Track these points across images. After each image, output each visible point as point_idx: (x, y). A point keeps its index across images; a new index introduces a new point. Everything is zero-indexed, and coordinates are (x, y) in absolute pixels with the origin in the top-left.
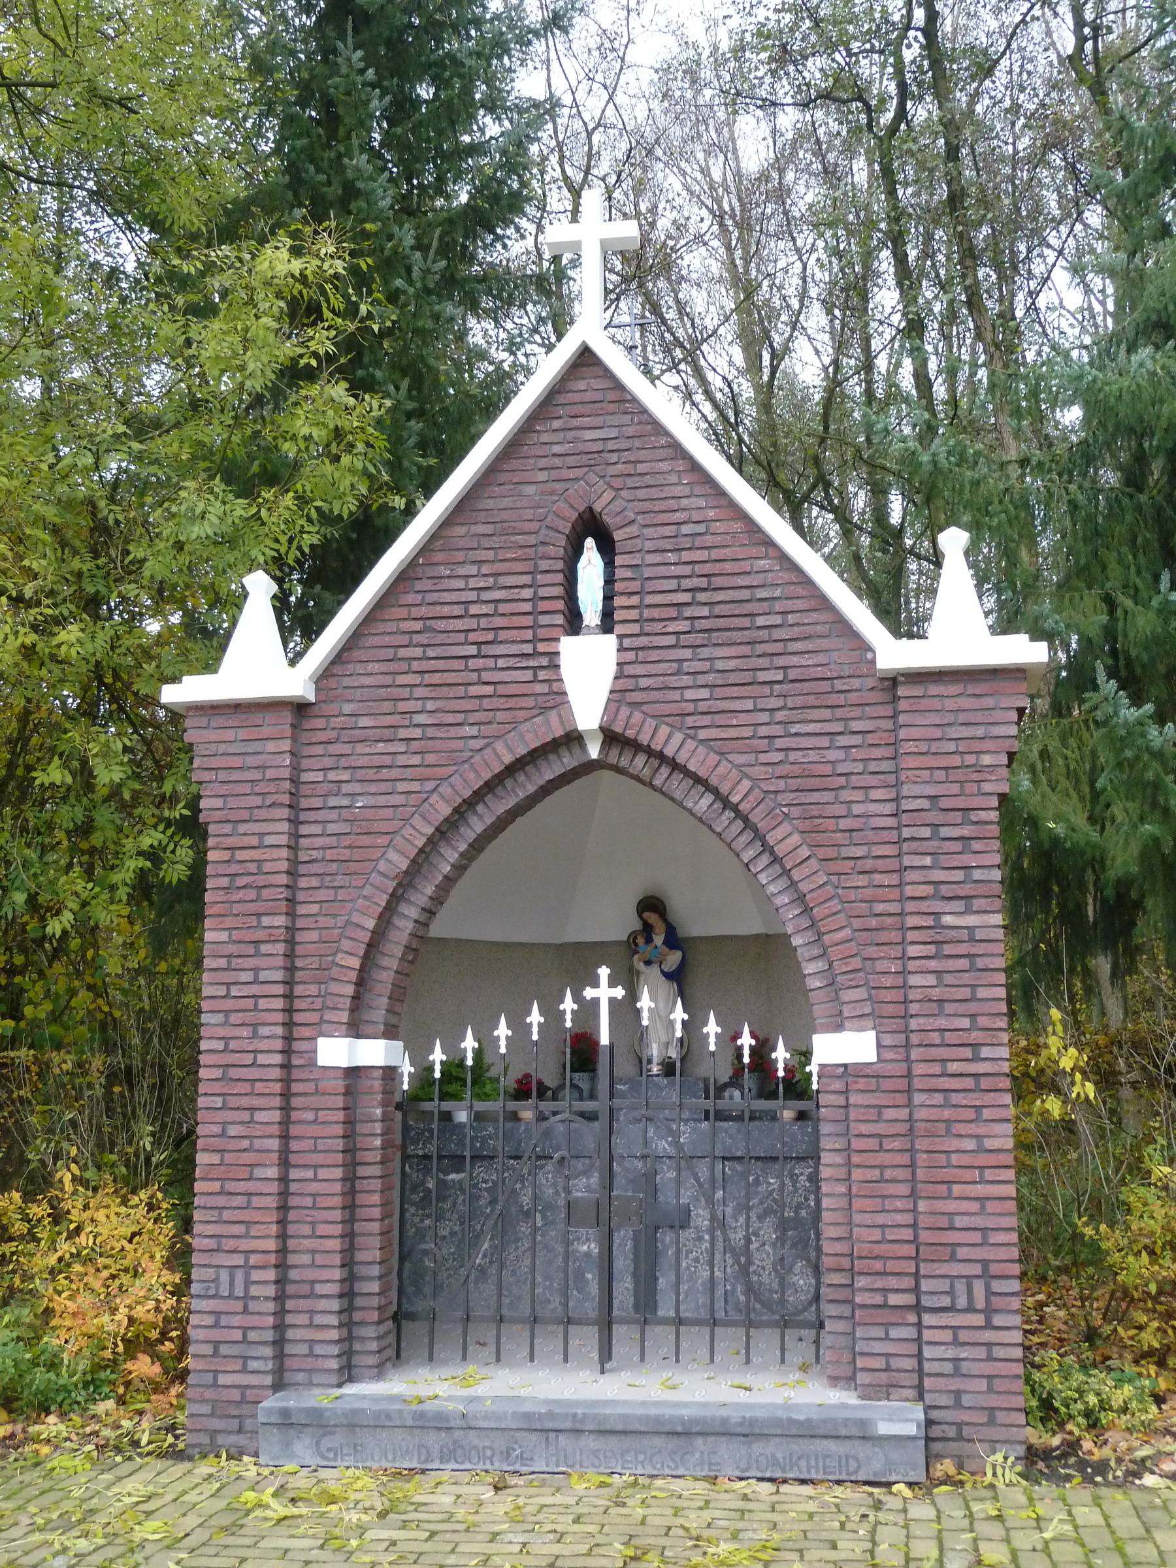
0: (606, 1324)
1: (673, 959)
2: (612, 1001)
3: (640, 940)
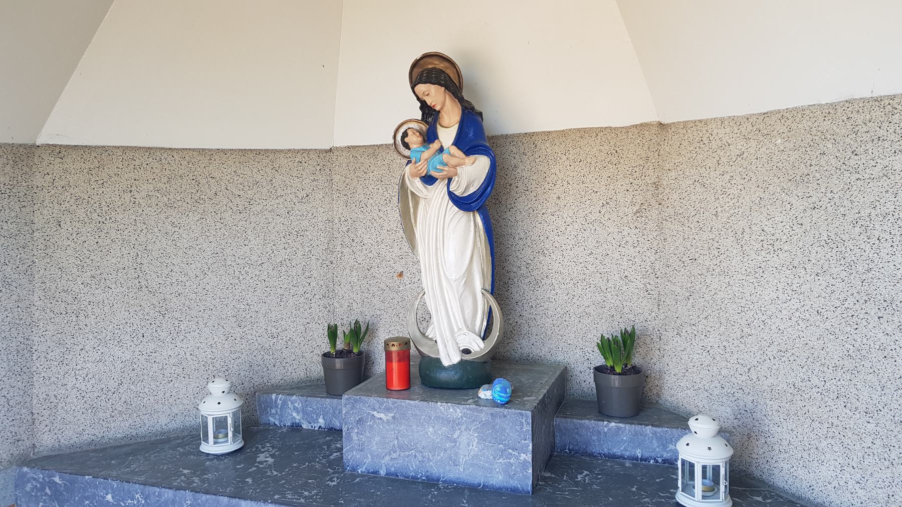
1: (473, 172)
3: (414, 140)
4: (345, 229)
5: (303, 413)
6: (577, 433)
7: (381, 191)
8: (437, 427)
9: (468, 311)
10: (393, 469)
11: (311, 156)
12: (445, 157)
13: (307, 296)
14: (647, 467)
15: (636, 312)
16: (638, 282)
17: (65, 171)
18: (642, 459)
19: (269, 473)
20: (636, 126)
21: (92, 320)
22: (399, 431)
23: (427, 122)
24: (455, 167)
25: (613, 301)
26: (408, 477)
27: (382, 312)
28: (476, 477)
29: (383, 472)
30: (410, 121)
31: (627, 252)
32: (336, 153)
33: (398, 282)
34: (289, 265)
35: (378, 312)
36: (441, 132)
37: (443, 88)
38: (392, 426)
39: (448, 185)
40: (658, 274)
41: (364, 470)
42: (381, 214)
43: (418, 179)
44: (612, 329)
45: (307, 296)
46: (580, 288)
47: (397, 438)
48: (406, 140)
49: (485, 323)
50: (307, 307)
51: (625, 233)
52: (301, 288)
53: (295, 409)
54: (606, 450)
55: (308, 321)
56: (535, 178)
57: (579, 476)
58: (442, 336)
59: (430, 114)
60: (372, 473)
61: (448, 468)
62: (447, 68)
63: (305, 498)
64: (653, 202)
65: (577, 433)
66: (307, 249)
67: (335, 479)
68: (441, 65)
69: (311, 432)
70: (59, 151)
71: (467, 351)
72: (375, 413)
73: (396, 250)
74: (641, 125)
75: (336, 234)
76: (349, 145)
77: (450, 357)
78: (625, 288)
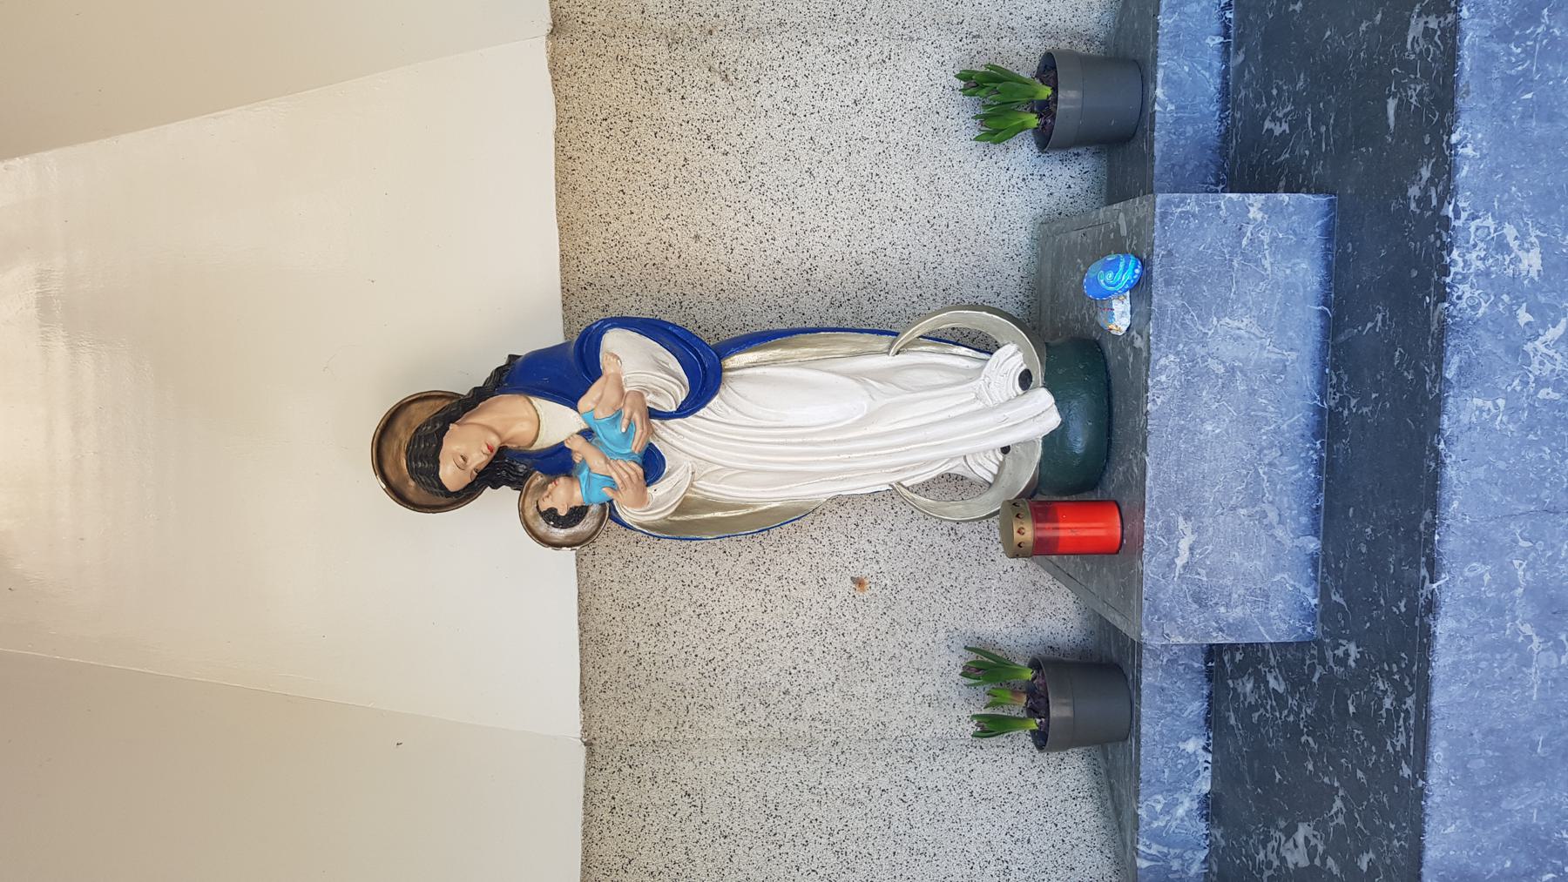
1: (634, 363)
3: (562, 495)
4: (761, 711)
5: (1177, 789)
6: (1182, 167)
7: (679, 627)
8: (1202, 413)
10: (1304, 520)
11: (599, 785)
13: (910, 796)
14: (1242, 19)
15: (925, 79)
16: (866, 80)
18: (1227, 36)
19: (1341, 820)
20: (554, 80)
22: (1217, 503)
23: (527, 476)
24: (623, 395)
25: (905, 129)
26: (1319, 483)
27: (940, 625)
28: (1307, 315)
29: (1313, 544)
30: (522, 511)
31: (806, 99)
32: (595, 732)
33: (875, 590)
34: (842, 836)
35: (942, 635)
36: (547, 440)
37: (452, 426)
38: (1207, 521)
39: (664, 416)
40: (849, 39)
41: (1309, 591)
42: (729, 627)
43: (650, 490)
44: (960, 116)
45: (910, 796)
46: (880, 195)
47: (1234, 508)
48: (562, 512)
49: (963, 350)
50: (935, 797)
51: (768, 104)
52: (893, 810)
53: (1169, 809)
54: (1213, 108)
55: (966, 795)
56: (655, 287)
57: (1278, 131)
58: (993, 435)
59: (505, 468)
60: (1316, 571)
61: (1292, 388)
62: (409, 423)
63: (1400, 700)
64: (707, 48)
65: (1182, 167)
66: (807, 795)
67: (1340, 652)
68: (403, 435)
69: (1221, 770)
71: (1025, 380)
72: (1180, 562)
73: (807, 593)
74: (552, 70)
75: (773, 733)
76: (577, 700)
77: (1039, 414)
78: (877, 105)
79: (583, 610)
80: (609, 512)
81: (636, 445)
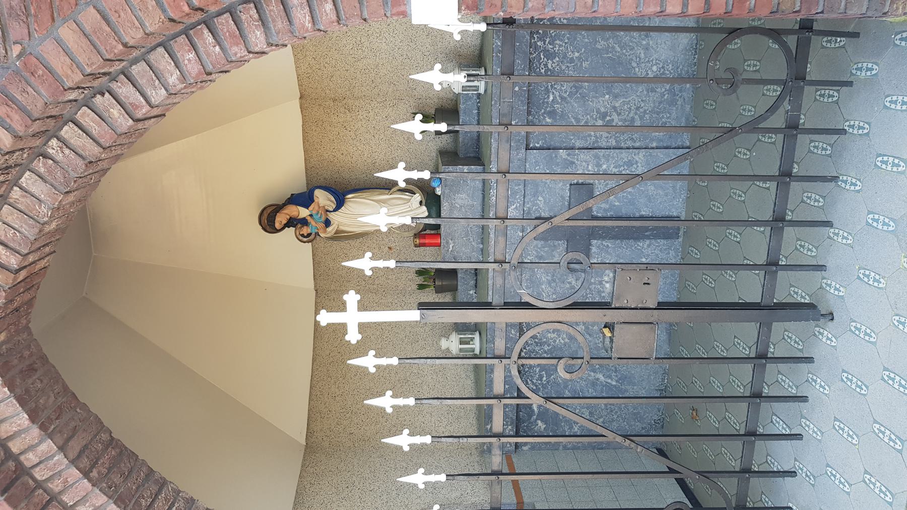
0: (770, 310)
1: (323, 198)
2: (363, 307)
3: (305, 231)
9: (399, 202)
12: (314, 213)
17: (321, 430)
21: (407, 418)
59: (292, 222)
68: (265, 215)
70: (310, 433)
71: (421, 203)
79: (313, 255)
80: (317, 234)
81: (323, 219)
